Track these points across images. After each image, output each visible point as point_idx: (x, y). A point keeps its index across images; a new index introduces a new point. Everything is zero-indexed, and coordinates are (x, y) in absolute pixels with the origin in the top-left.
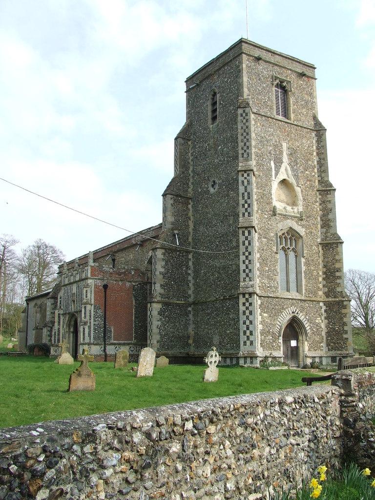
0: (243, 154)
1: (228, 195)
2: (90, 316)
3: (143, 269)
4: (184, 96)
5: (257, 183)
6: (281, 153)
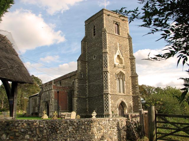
1: (99, 60)
6: (117, 46)
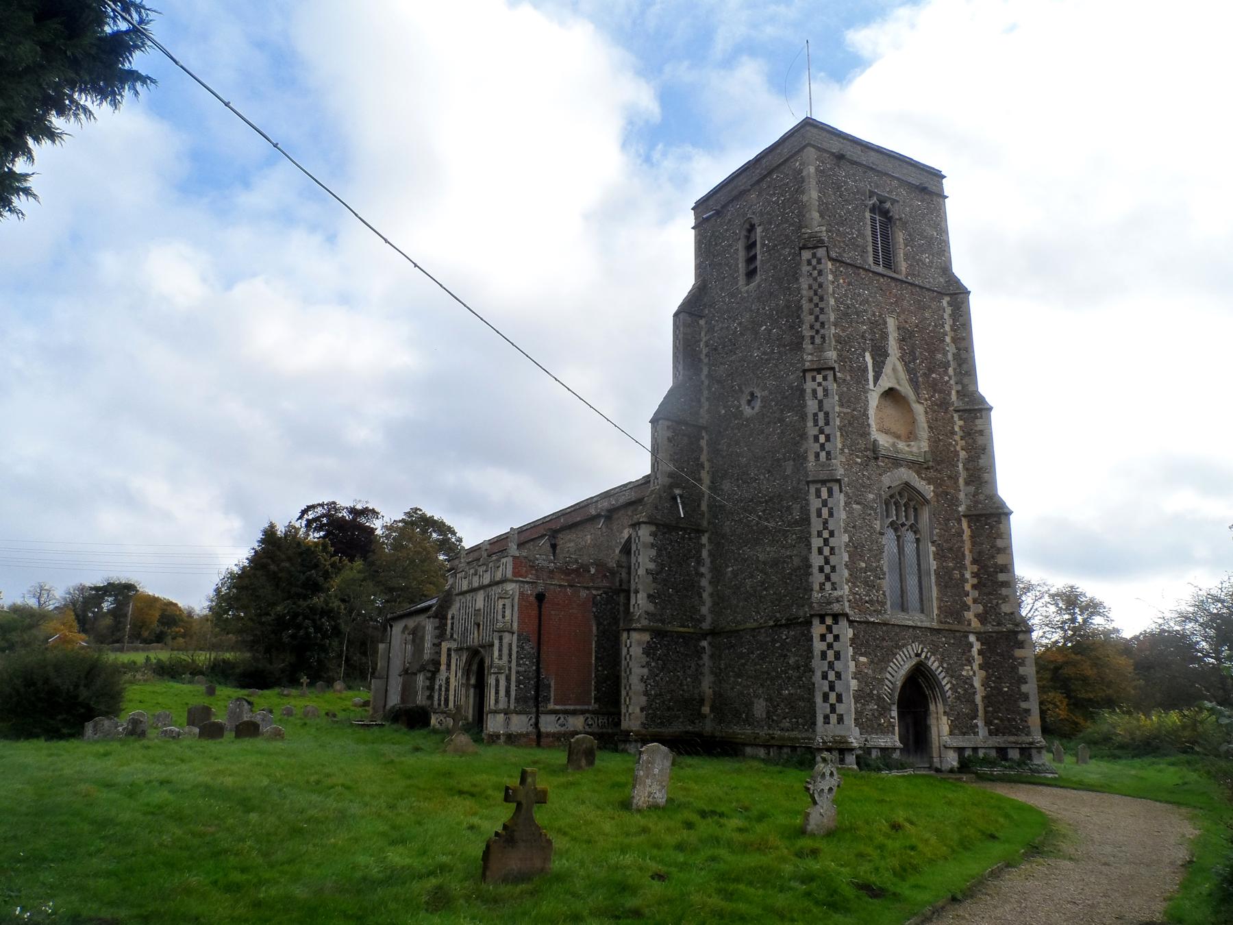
0: (812, 338)
1: (781, 420)
2: (510, 655)
3: (612, 564)
4: (691, 235)
5: (841, 396)
6: (885, 336)
